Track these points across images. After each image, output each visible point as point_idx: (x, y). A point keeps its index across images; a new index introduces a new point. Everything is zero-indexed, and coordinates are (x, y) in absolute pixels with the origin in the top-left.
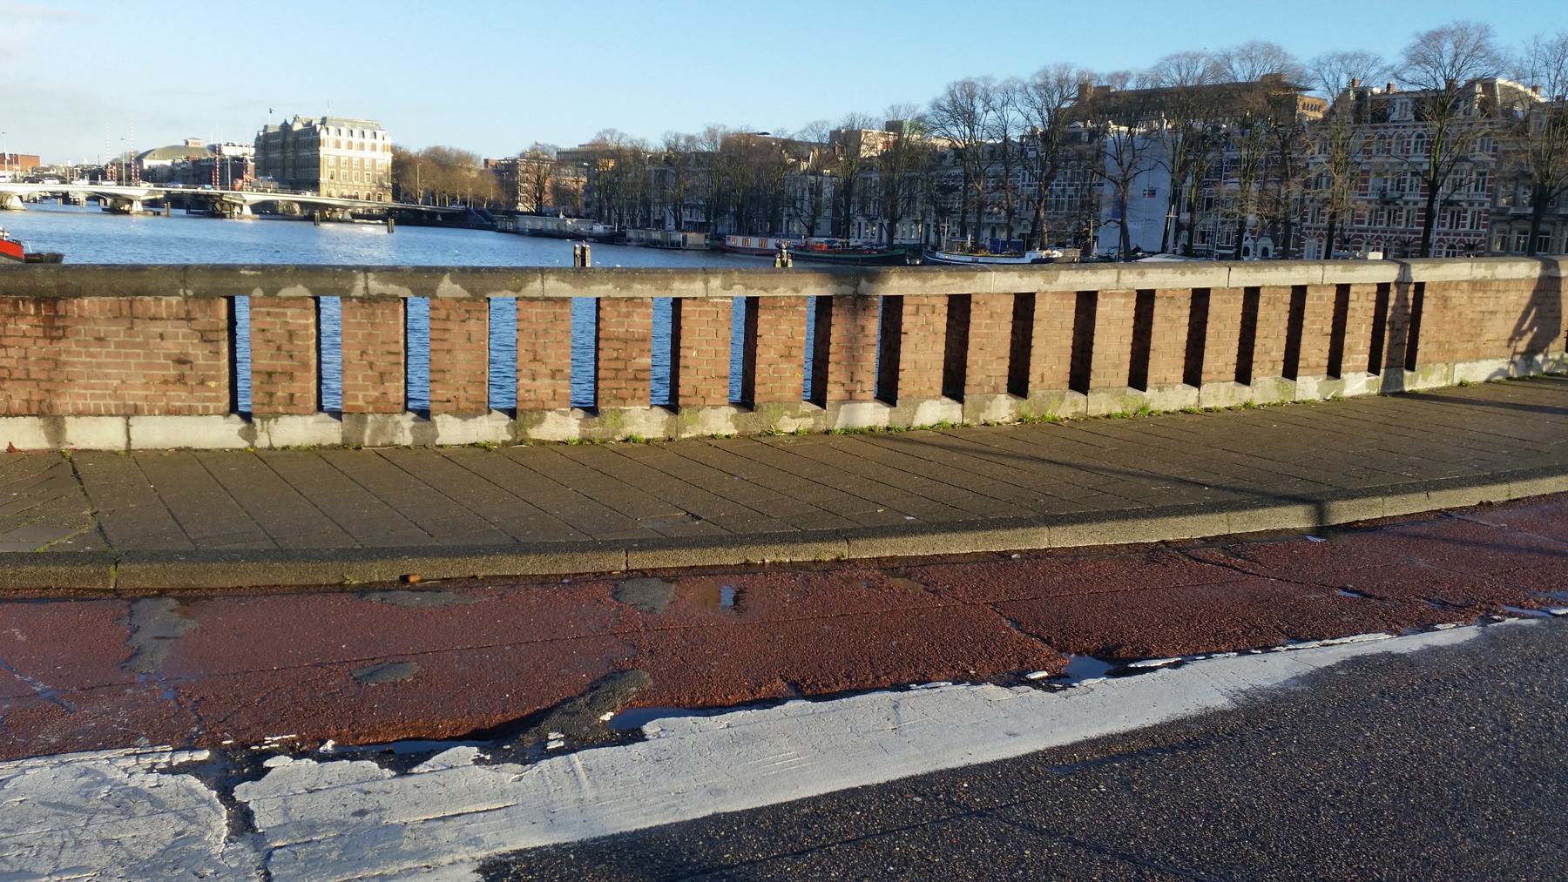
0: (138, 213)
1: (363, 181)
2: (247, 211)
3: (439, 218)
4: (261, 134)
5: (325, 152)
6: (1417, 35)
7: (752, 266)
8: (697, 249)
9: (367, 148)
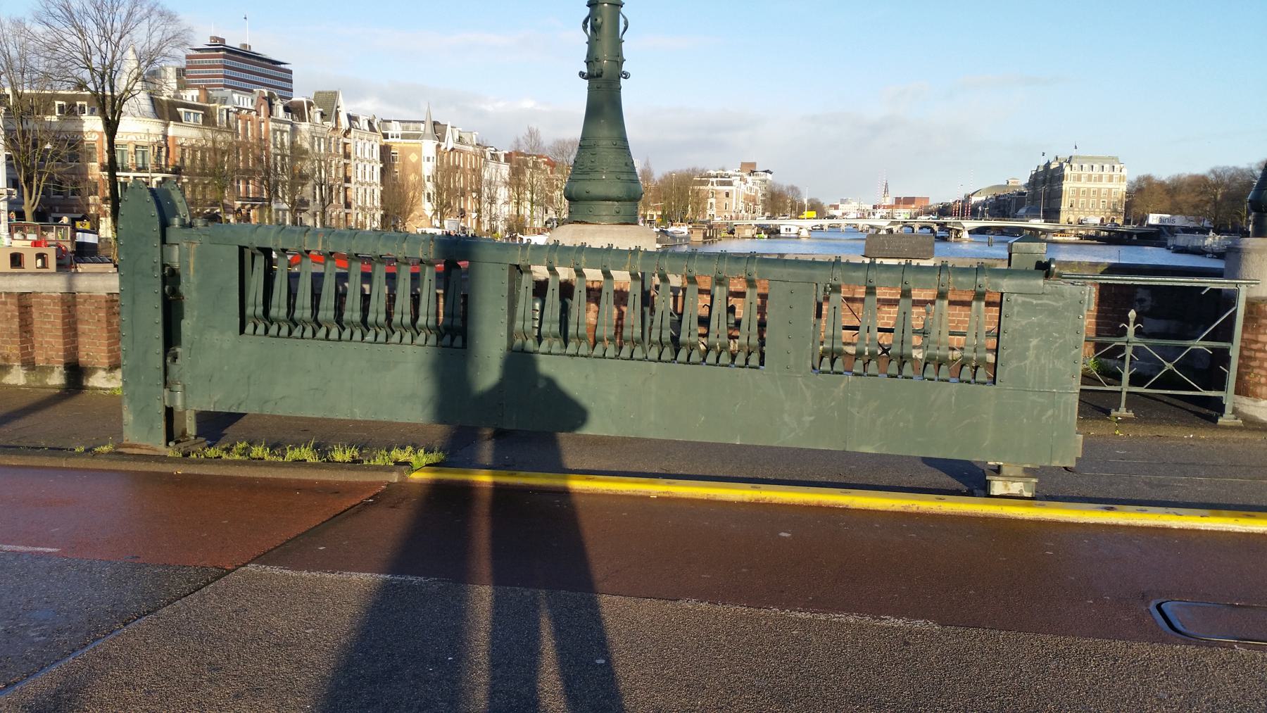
4: (1034, 173)
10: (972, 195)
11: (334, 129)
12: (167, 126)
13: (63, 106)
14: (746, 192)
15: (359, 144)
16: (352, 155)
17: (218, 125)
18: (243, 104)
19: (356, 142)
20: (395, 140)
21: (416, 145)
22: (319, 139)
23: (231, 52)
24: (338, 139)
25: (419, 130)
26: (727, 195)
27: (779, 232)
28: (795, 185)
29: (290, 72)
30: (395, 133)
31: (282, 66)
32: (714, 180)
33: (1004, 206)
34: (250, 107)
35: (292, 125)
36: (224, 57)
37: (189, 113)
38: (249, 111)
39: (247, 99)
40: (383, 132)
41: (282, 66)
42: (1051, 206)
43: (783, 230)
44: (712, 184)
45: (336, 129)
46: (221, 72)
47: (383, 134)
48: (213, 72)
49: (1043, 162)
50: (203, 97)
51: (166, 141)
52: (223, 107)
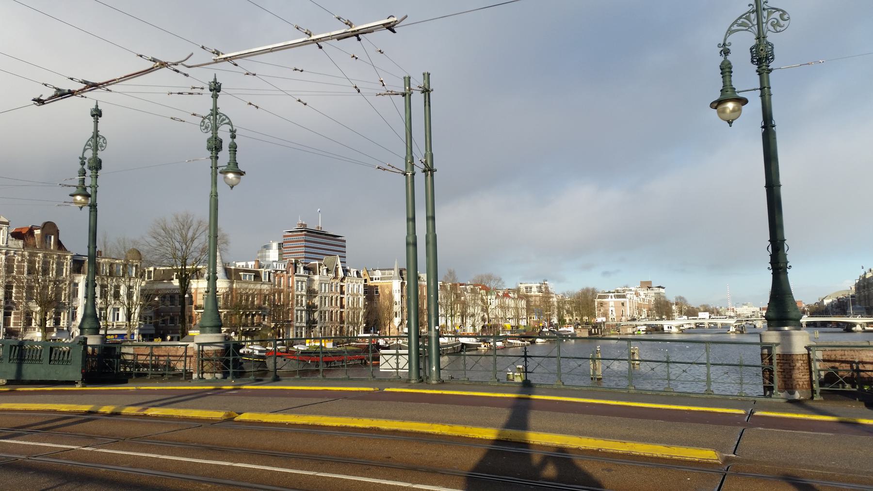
0: (732, 332)
4: (857, 281)
10: (824, 299)
11: (334, 278)
12: (232, 283)
13: (15, 317)
14: (640, 302)
15: (350, 286)
16: (346, 292)
17: (263, 280)
18: (279, 268)
19: (349, 284)
20: (377, 281)
21: (389, 284)
22: (325, 284)
23: (310, 232)
24: (337, 283)
25: (391, 274)
26: (623, 304)
27: (663, 329)
28: (682, 296)
29: (344, 241)
30: (377, 277)
31: (340, 238)
32: (613, 294)
33: (844, 306)
34: (283, 269)
35: (308, 277)
36: (305, 235)
37: (246, 275)
38: (282, 271)
39: (282, 265)
40: (371, 277)
41: (340, 238)
42: (871, 305)
43: (666, 328)
44: (612, 297)
45: (336, 278)
46: (303, 244)
47: (370, 278)
48: (299, 244)
49: (862, 273)
50: (257, 266)
51: (232, 292)
52: (266, 270)
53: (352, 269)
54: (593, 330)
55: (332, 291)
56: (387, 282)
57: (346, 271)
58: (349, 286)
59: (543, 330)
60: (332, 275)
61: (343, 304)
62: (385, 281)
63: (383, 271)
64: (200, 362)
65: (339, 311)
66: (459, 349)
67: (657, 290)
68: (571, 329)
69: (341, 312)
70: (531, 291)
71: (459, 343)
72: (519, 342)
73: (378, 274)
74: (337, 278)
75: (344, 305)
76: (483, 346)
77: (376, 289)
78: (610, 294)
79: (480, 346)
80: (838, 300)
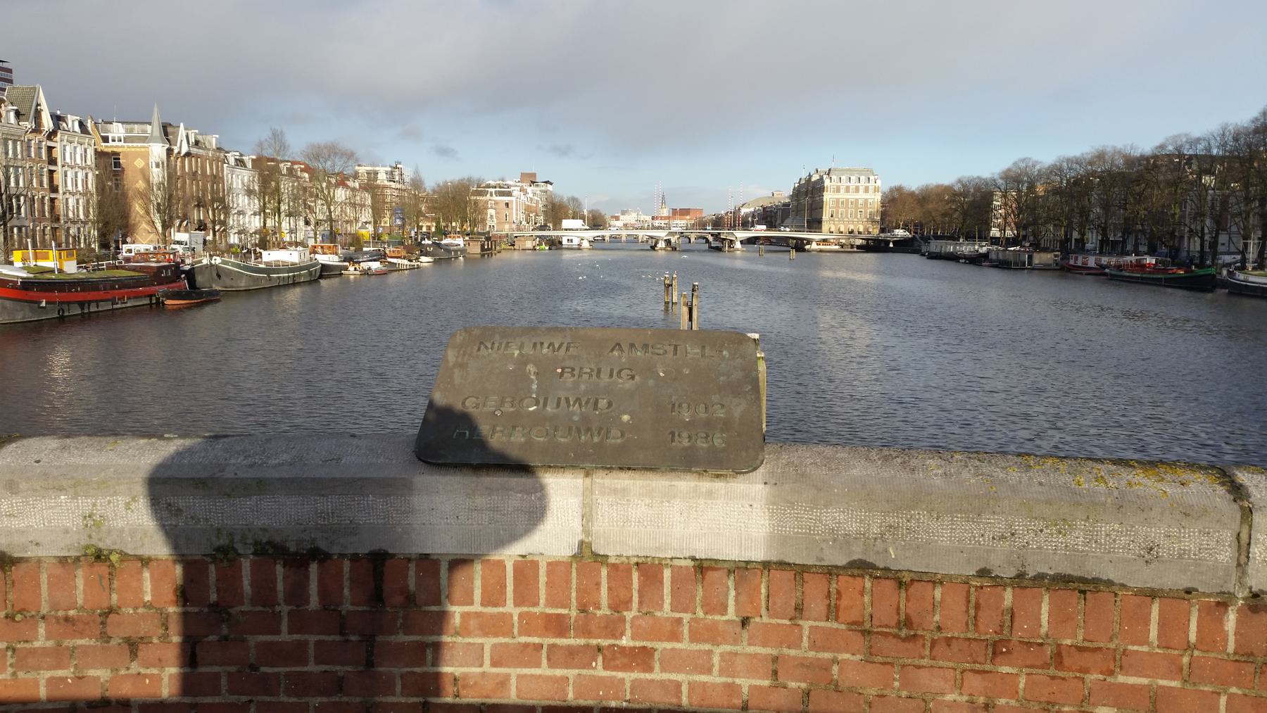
0: (661, 249)
1: (856, 217)
2: (738, 245)
3: (891, 245)
4: (797, 185)
5: (827, 197)
6: (1093, 148)
7: (149, 699)
8: (1045, 269)
9: (861, 190)
11: (34, 131)
19: (64, 146)
20: (116, 143)
21: (143, 150)
22: (15, 142)
27: (560, 243)
29: (10, 71)
30: (116, 136)
32: (493, 190)
43: (565, 242)
44: (491, 195)
45: (37, 130)
47: (102, 137)
53: (69, 116)
54: (486, 243)
55: (29, 156)
56: (137, 147)
57: (57, 119)
58: (65, 150)
59: (423, 242)
60: (28, 125)
61: (55, 183)
62: (135, 145)
63: (129, 126)
64: (798, 435)
65: (47, 198)
66: (318, 274)
67: (543, 187)
68: (460, 241)
69: (52, 200)
70: (376, 179)
71: (318, 264)
72: (406, 262)
73: (117, 130)
74: (40, 132)
75: (57, 186)
76: (351, 268)
77: (114, 159)
78: (490, 190)
79: (346, 268)
80: (764, 209)
